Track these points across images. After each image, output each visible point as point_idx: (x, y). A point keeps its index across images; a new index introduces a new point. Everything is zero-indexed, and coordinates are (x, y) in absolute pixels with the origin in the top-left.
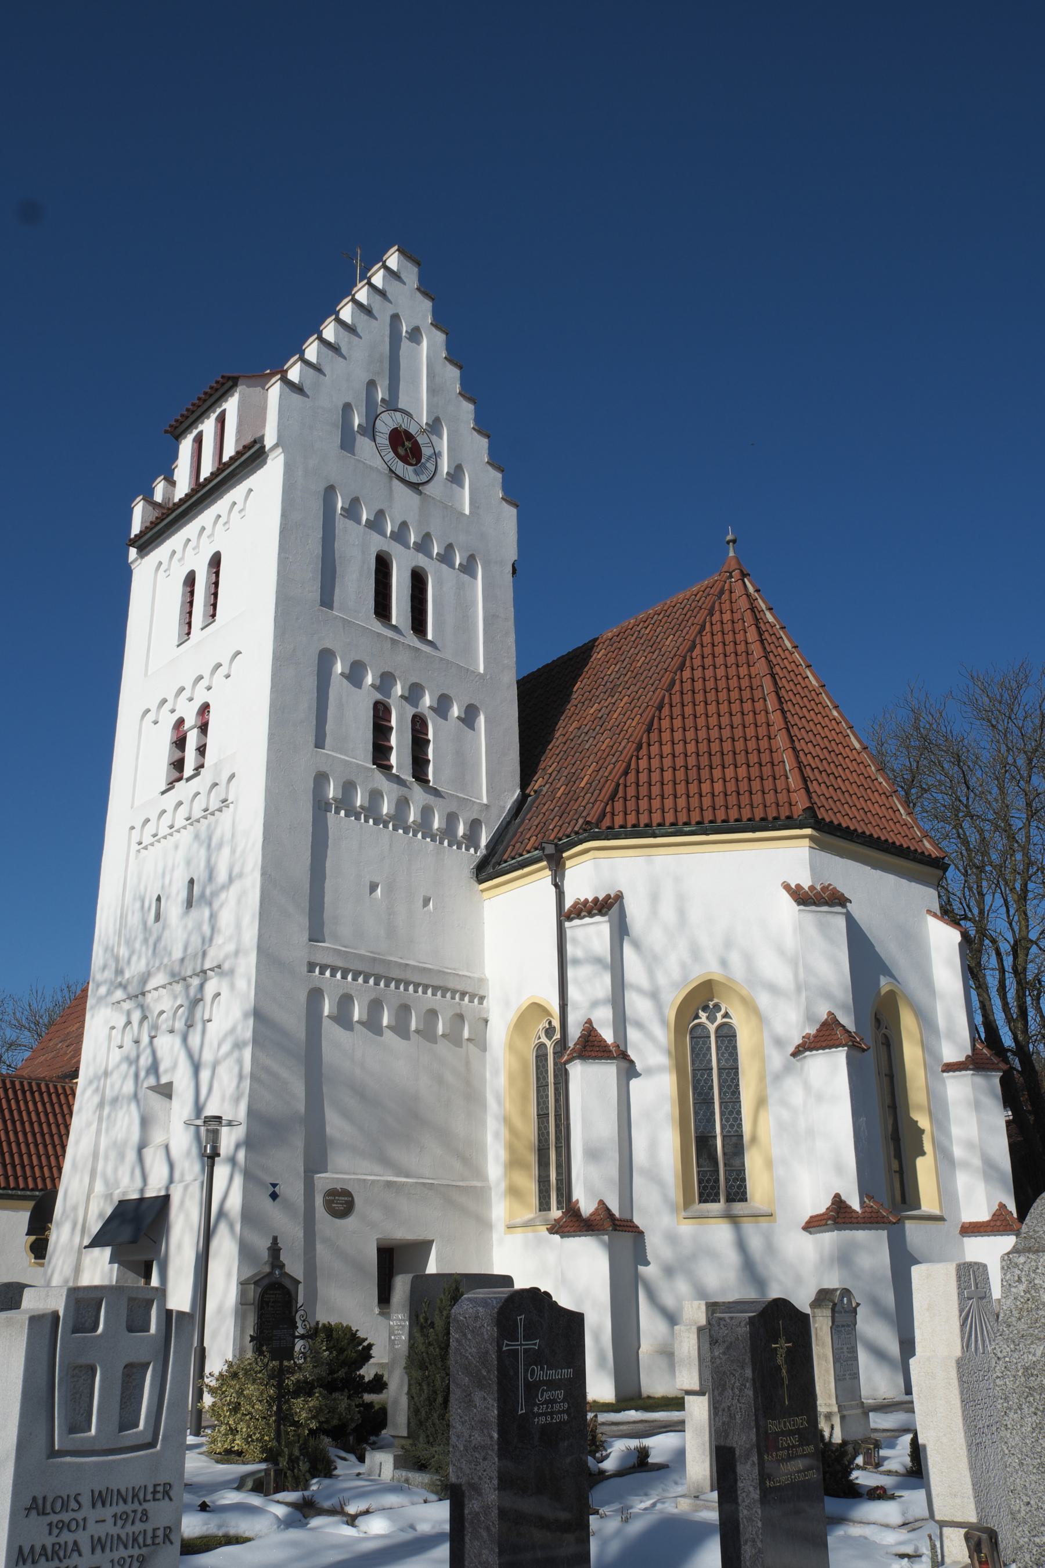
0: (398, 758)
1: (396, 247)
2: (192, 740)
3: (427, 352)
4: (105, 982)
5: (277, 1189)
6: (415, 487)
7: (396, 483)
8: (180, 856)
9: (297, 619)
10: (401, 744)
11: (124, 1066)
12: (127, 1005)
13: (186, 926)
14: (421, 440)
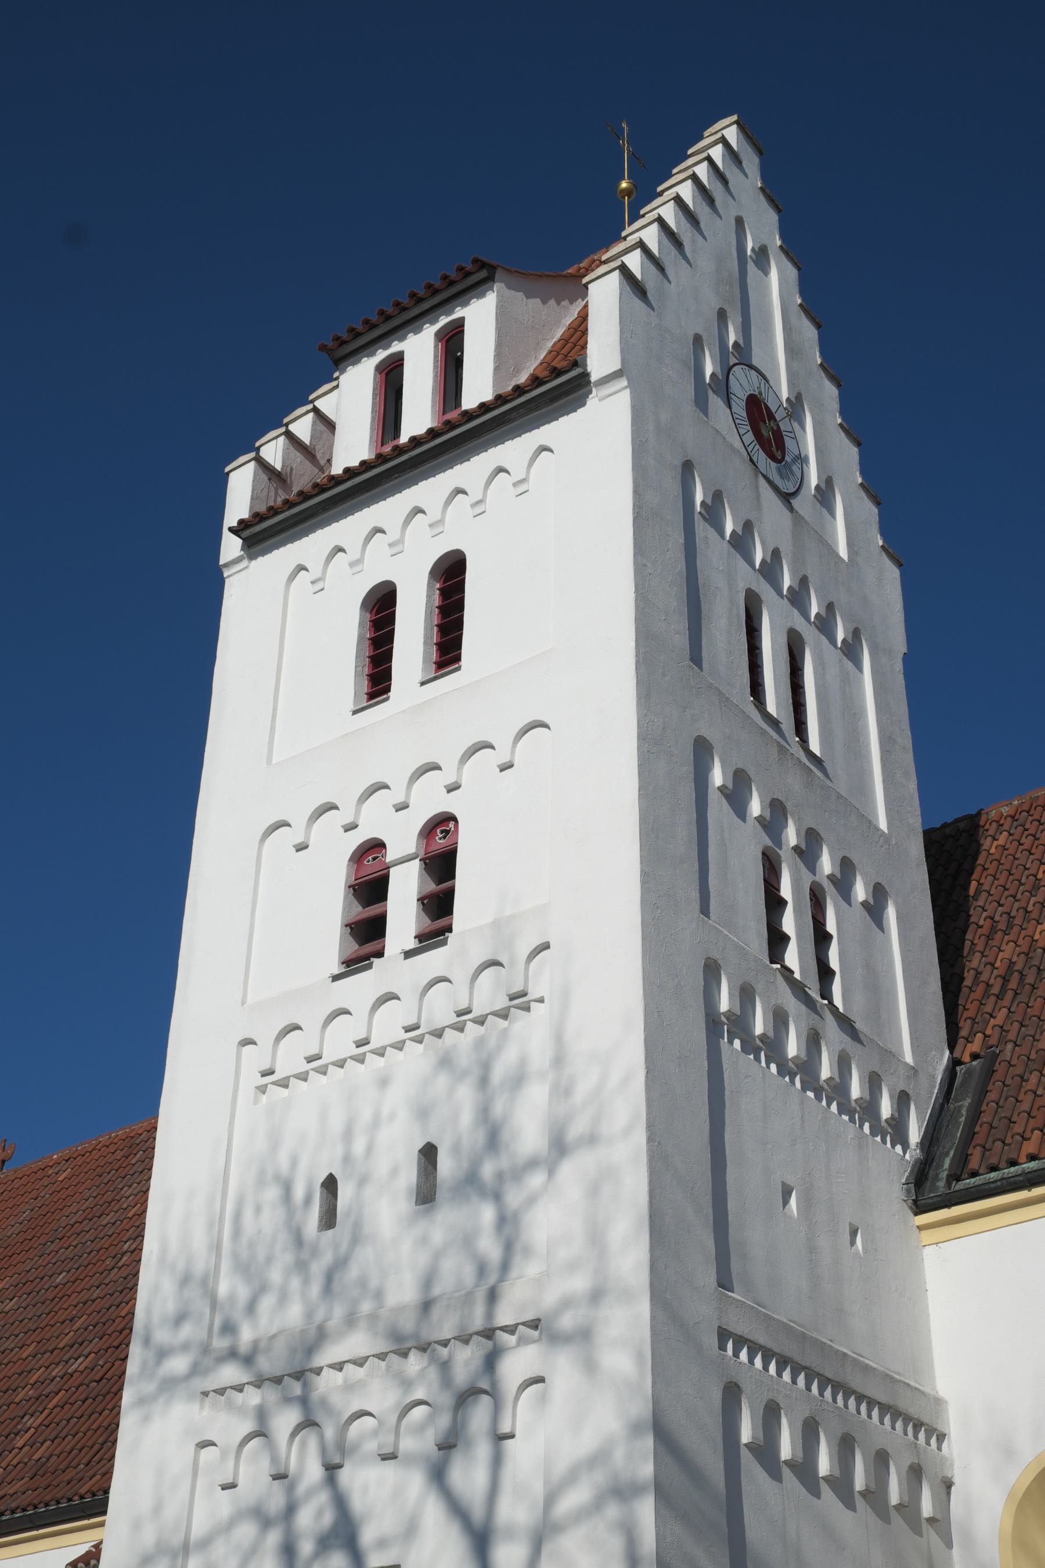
1: (735, 118)
3: (776, 285)
4: (185, 1347)
8: (397, 1099)
9: (664, 675)
11: (247, 1531)
12: (253, 1397)
13: (424, 1240)
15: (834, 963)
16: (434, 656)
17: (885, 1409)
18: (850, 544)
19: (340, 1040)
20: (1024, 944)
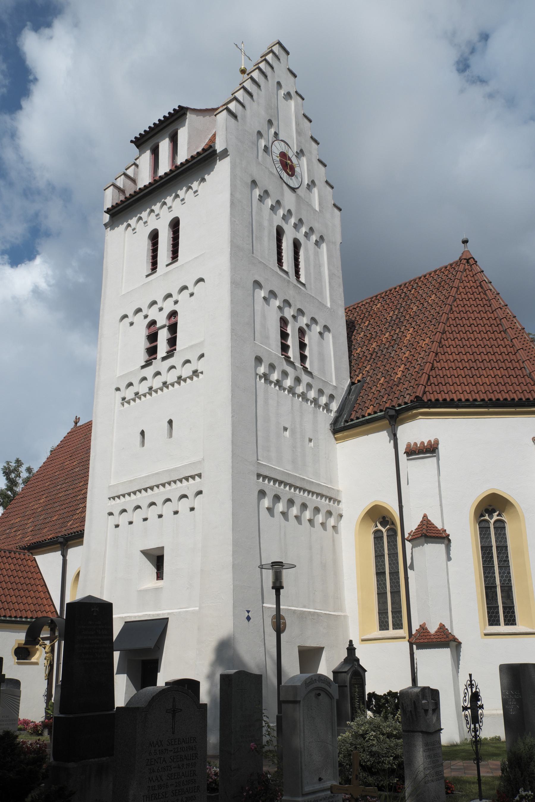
0: (293, 353)
2: (163, 335)
5: (250, 614)
6: (293, 189)
7: (284, 185)
14: (294, 160)
15: (307, 353)
16: (171, 256)
17: (318, 494)
18: (320, 204)
19: (143, 388)
20: (379, 342)
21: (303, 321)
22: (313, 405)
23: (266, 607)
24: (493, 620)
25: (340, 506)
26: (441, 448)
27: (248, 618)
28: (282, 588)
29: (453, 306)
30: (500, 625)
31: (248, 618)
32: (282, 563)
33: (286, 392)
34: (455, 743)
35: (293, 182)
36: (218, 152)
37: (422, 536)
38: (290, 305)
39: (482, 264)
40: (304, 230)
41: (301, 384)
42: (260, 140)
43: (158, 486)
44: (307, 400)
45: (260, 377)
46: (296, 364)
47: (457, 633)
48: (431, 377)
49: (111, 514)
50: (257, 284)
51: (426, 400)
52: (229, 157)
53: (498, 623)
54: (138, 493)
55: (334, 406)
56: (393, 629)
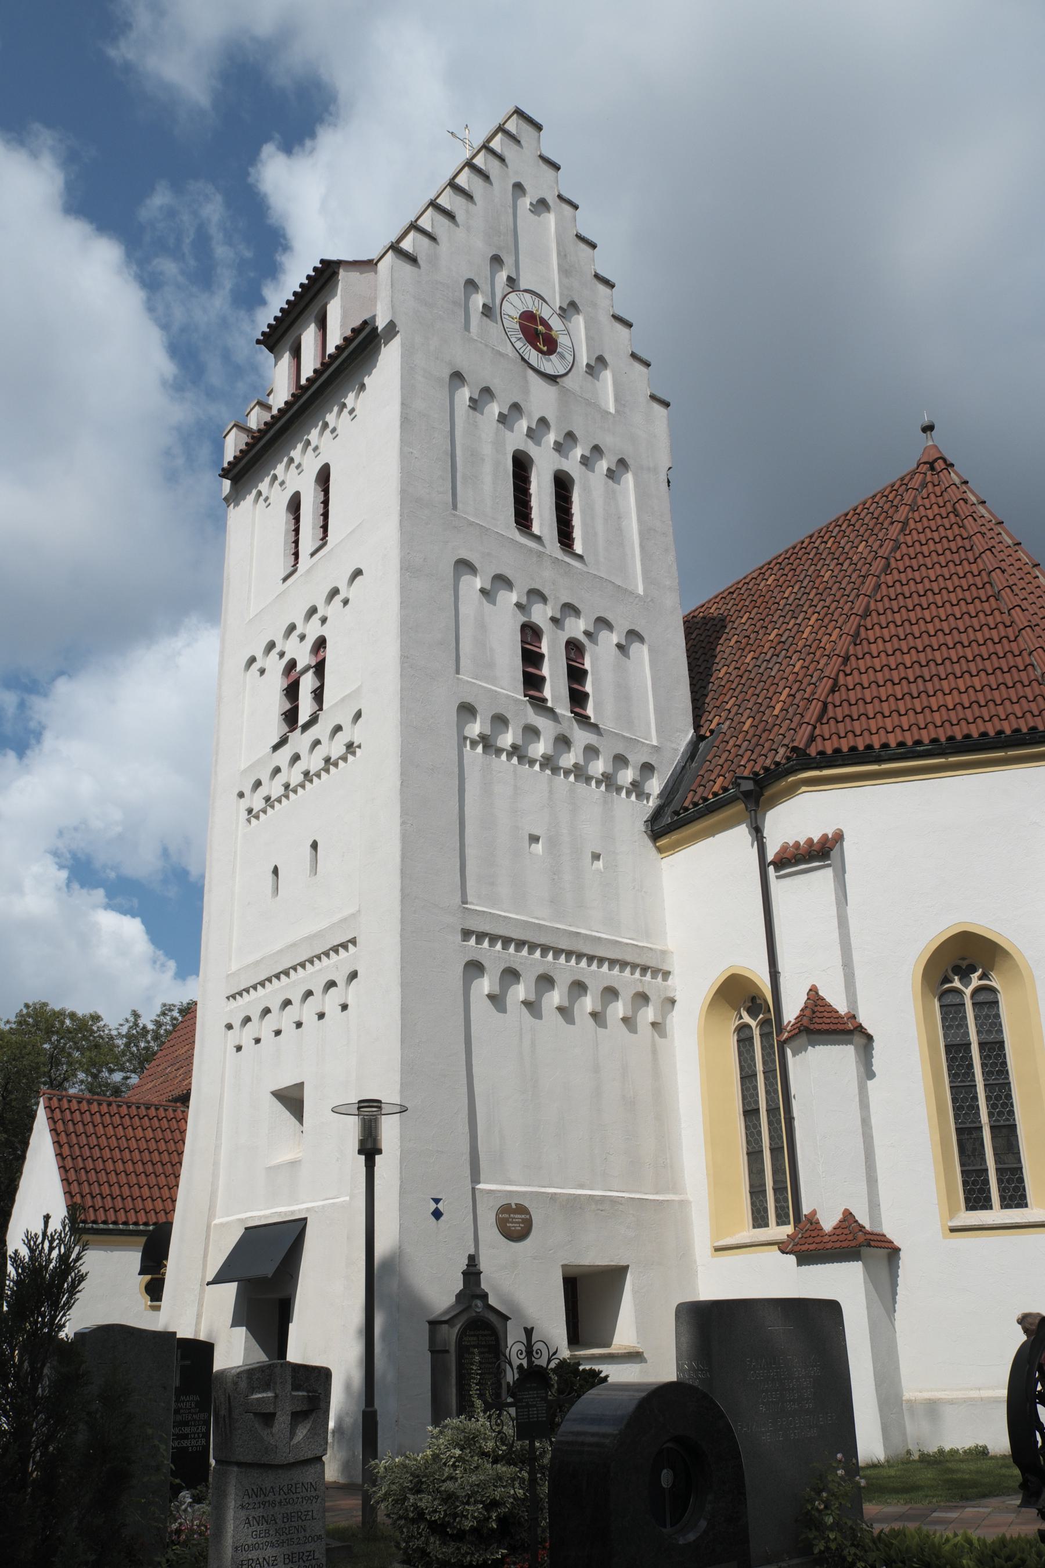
0: (555, 688)
2: (307, 684)
5: (440, 1206)
6: (553, 379)
7: (530, 372)
10: (553, 672)
14: (556, 323)
18: (617, 400)
21: (576, 627)
22: (603, 788)
23: (482, 1190)
24: (976, 1199)
25: (670, 982)
26: (849, 847)
27: (437, 1214)
28: (380, 1152)
29: (892, 561)
30: (991, 1208)
31: (437, 1214)
32: (379, 1101)
33: (537, 767)
34: (875, 1461)
35: (552, 365)
36: (379, 329)
37: (800, 1031)
38: (544, 599)
39: (963, 468)
40: (578, 452)
41: (572, 749)
42: (474, 296)
43: (295, 968)
44: (588, 779)
45: (474, 744)
46: (558, 711)
47: (890, 1230)
48: (830, 707)
49: (229, 1027)
50: (465, 566)
51: (813, 754)
52: (398, 336)
53: (987, 1205)
54: (267, 983)
55: (655, 786)
56: (778, 1224)
